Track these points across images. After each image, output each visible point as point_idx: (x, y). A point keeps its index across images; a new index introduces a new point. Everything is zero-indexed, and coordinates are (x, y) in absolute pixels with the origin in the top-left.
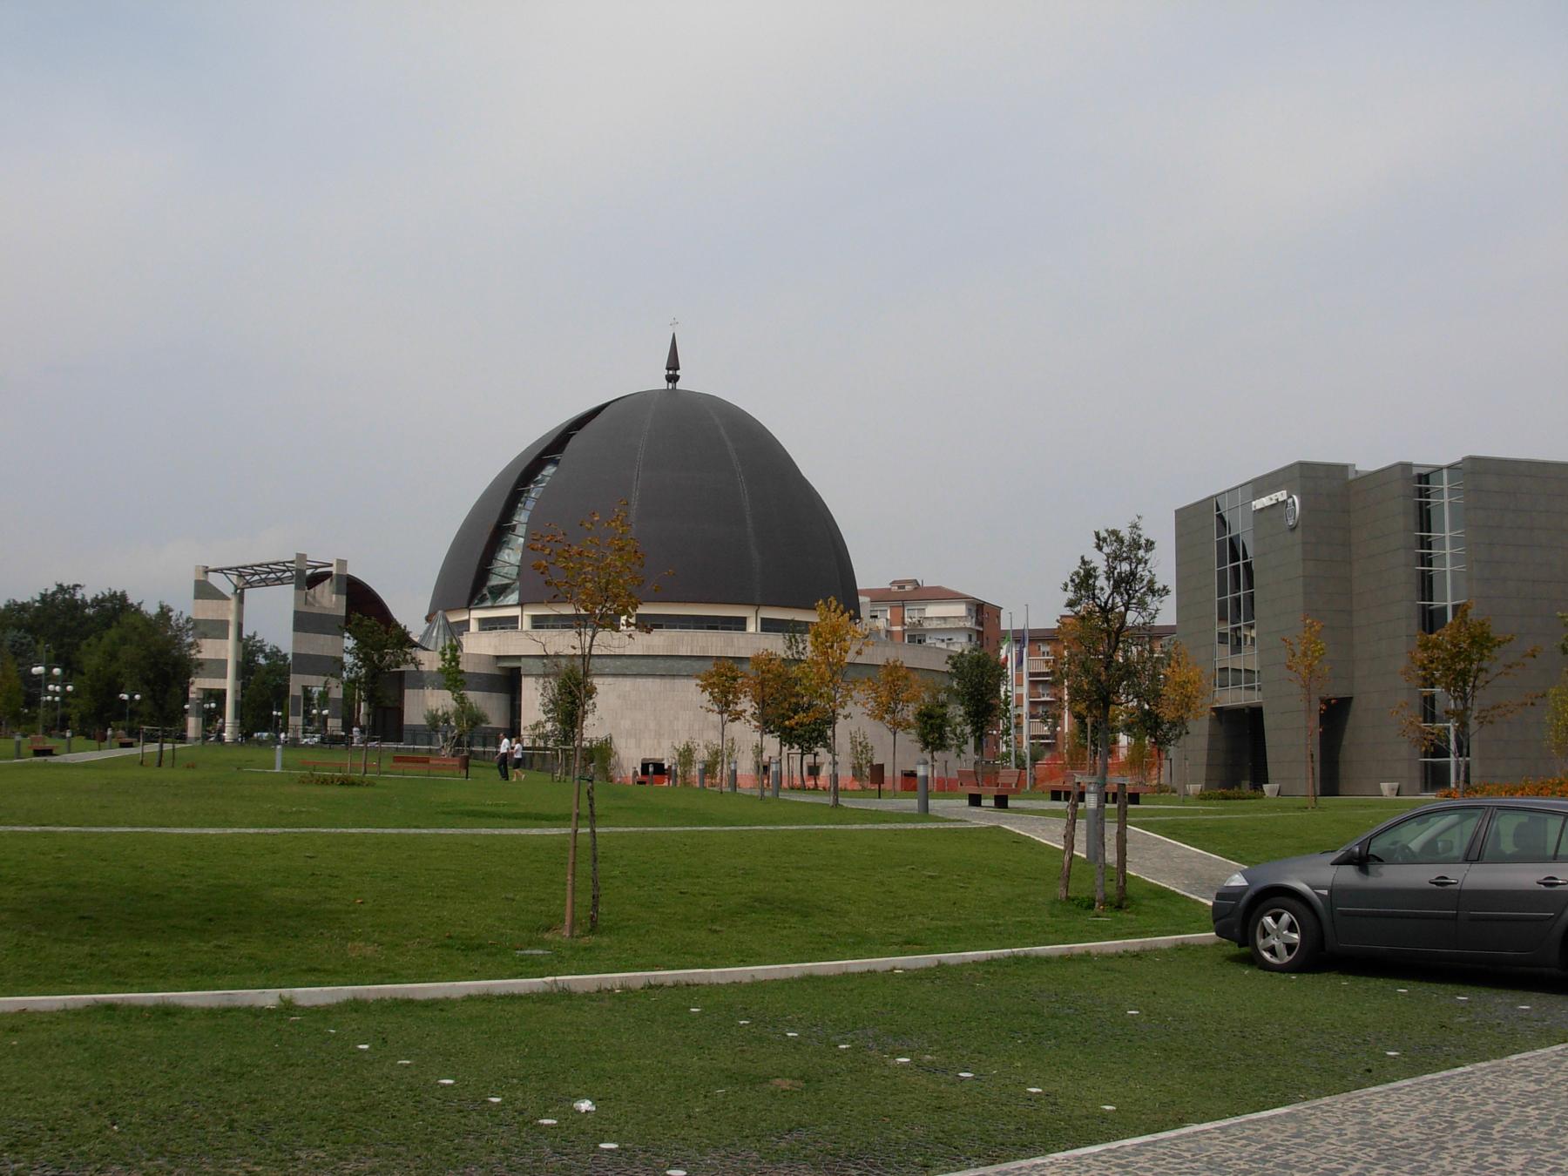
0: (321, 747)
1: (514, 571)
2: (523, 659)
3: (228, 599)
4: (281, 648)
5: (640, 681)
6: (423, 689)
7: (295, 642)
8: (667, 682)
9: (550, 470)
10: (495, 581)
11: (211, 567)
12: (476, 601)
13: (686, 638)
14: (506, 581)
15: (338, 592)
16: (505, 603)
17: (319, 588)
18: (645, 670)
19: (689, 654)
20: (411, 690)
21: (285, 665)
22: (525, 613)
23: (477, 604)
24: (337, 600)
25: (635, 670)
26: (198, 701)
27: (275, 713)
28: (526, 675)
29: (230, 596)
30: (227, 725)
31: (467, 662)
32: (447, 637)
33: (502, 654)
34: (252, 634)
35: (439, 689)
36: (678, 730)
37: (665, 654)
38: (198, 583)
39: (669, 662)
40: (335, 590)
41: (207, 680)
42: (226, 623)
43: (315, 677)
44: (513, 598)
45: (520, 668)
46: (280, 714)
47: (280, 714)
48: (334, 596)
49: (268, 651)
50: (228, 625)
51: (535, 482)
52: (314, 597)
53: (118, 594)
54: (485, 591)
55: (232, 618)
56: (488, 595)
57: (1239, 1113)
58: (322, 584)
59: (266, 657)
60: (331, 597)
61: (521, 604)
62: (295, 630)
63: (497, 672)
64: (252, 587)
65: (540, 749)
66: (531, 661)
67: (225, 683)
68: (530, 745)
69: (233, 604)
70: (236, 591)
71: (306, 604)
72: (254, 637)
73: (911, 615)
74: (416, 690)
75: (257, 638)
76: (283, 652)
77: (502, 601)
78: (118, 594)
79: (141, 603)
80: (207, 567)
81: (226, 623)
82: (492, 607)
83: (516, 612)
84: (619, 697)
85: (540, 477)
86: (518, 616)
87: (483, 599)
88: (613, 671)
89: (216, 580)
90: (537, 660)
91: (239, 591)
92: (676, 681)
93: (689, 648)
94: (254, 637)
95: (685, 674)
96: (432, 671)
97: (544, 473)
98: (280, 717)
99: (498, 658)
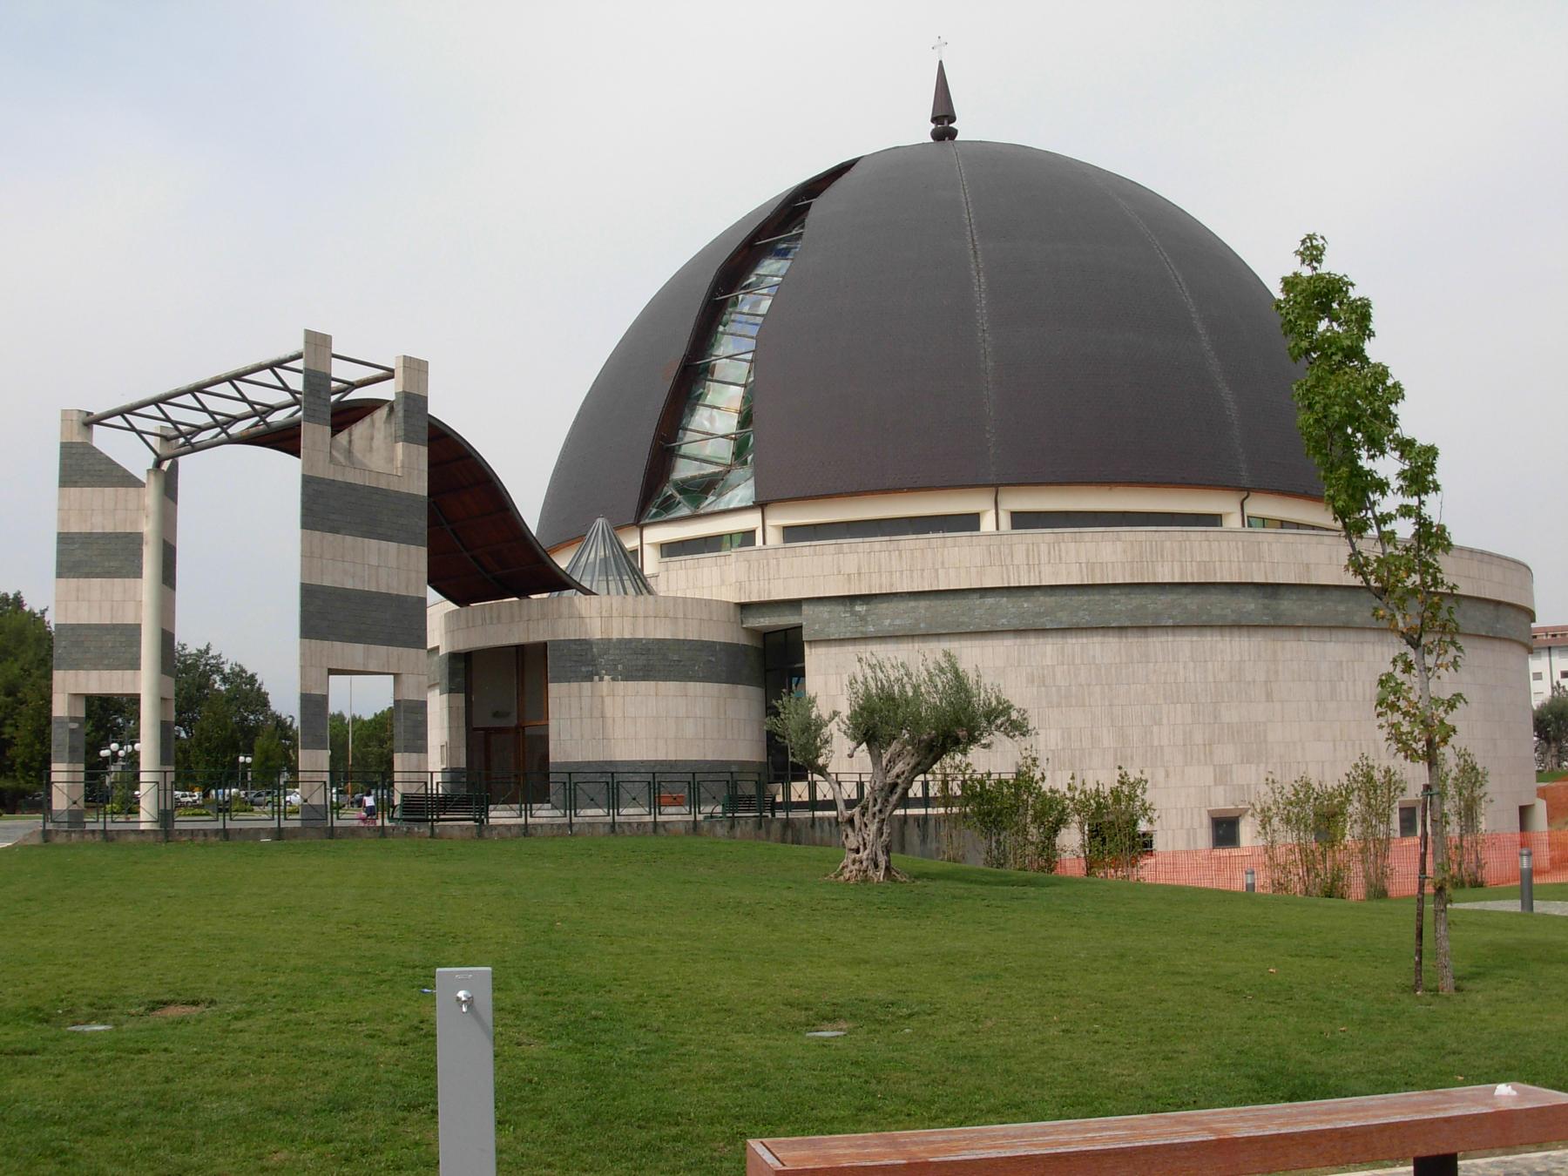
0: (409, 832)
1: (724, 451)
2: (805, 608)
3: (137, 483)
4: (246, 667)
5: (1074, 644)
6: (592, 680)
7: (307, 556)
8: (1133, 642)
9: (772, 269)
10: (684, 470)
11: (97, 411)
12: (654, 511)
13: (1168, 544)
14: (710, 469)
15: (409, 438)
16: (722, 507)
17: (360, 429)
18: (1084, 618)
19: (1177, 580)
20: (565, 685)
21: (252, 690)
22: (768, 522)
23: (656, 515)
24: (407, 454)
25: (1065, 618)
26: (75, 726)
27: (241, 759)
28: (814, 642)
29: (143, 477)
30: (143, 777)
31: (685, 617)
32: (625, 577)
33: (755, 599)
34: (203, 648)
35: (626, 679)
36: (1162, 747)
37: (1128, 581)
38: (67, 450)
39: (1137, 599)
40: (401, 433)
41: (94, 673)
42: (136, 540)
43: (360, 647)
44: (742, 493)
45: (800, 627)
46: (249, 760)
47: (249, 760)
48: (400, 446)
49: (227, 670)
50: (141, 544)
51: (745, 288)
52: (349, 452)
53: (11, 596)
54: (669, 490)
55: (148, 528)
56: (679, 497)
57: (310, 809)
58: (368, 419)
59: (225, 680)
60: (393, 450)
61: (761, 505)
62: (306, 525)
63: (742, 639)
64: (195, 448)
65: (800, 805)
66: (824, 611)
67: (136, 682)
68: (806, 798)
69: (150, 496)
70: (158, 464)
71: (331, 461)
72: (207, 651)
73: (1387, 528)
74: (575, 685)
75: (211, 653)
76: (249, 673)
77: (710, 503)
78: (11, 596)
79: (46, 610)
80: (89, 414)
81: (136, 540)
82: (695, 517)
83: (751, 521)
84: (1031, 680)
85: (753, 279)
86: (753, 532)
87: (668, 505)
88: (1016, 624)
89: (112, 443)
90: (840, 609)
91: (166, 465)
92: (1150, 639)
93: (1177, 566)
94: (207, 651)
95: (1170, 623)
96: (610, 640)
97: (761, 271)
98: (249, 765)
99: (744, 607)
